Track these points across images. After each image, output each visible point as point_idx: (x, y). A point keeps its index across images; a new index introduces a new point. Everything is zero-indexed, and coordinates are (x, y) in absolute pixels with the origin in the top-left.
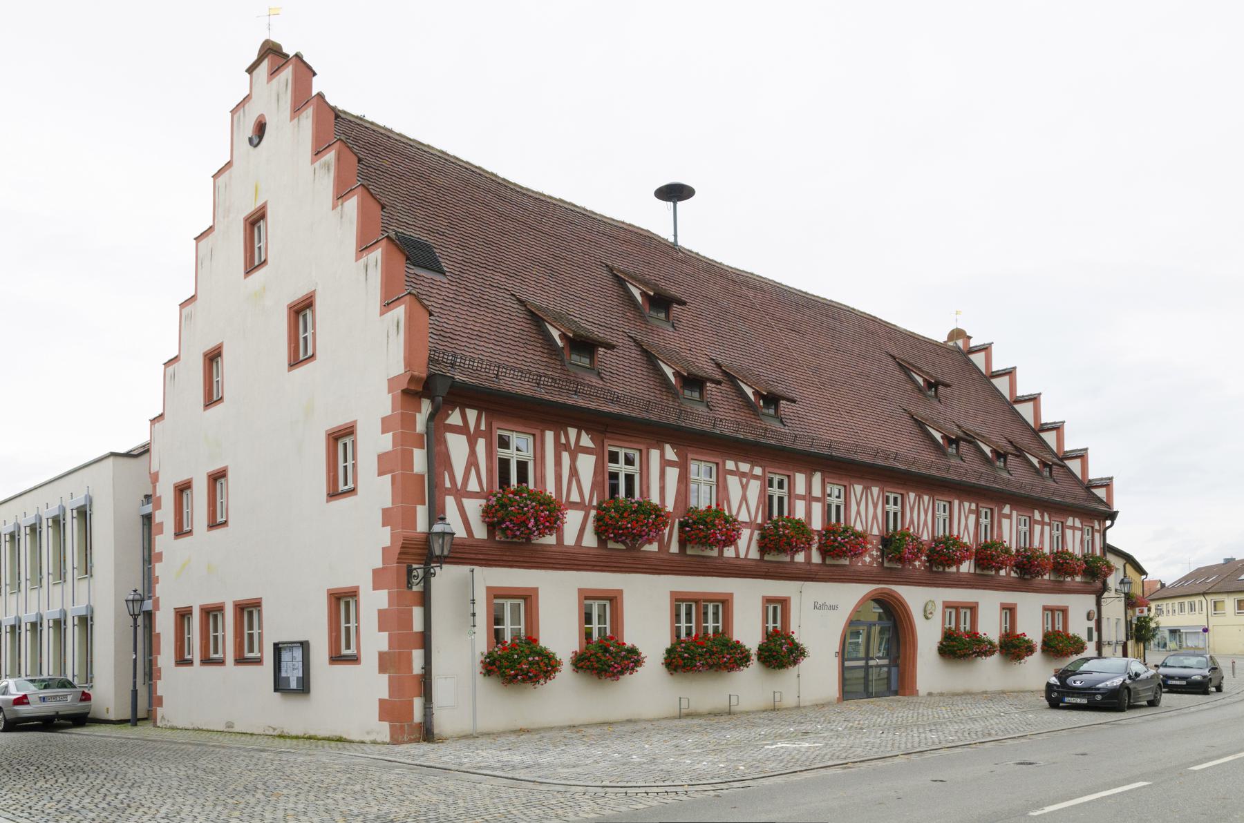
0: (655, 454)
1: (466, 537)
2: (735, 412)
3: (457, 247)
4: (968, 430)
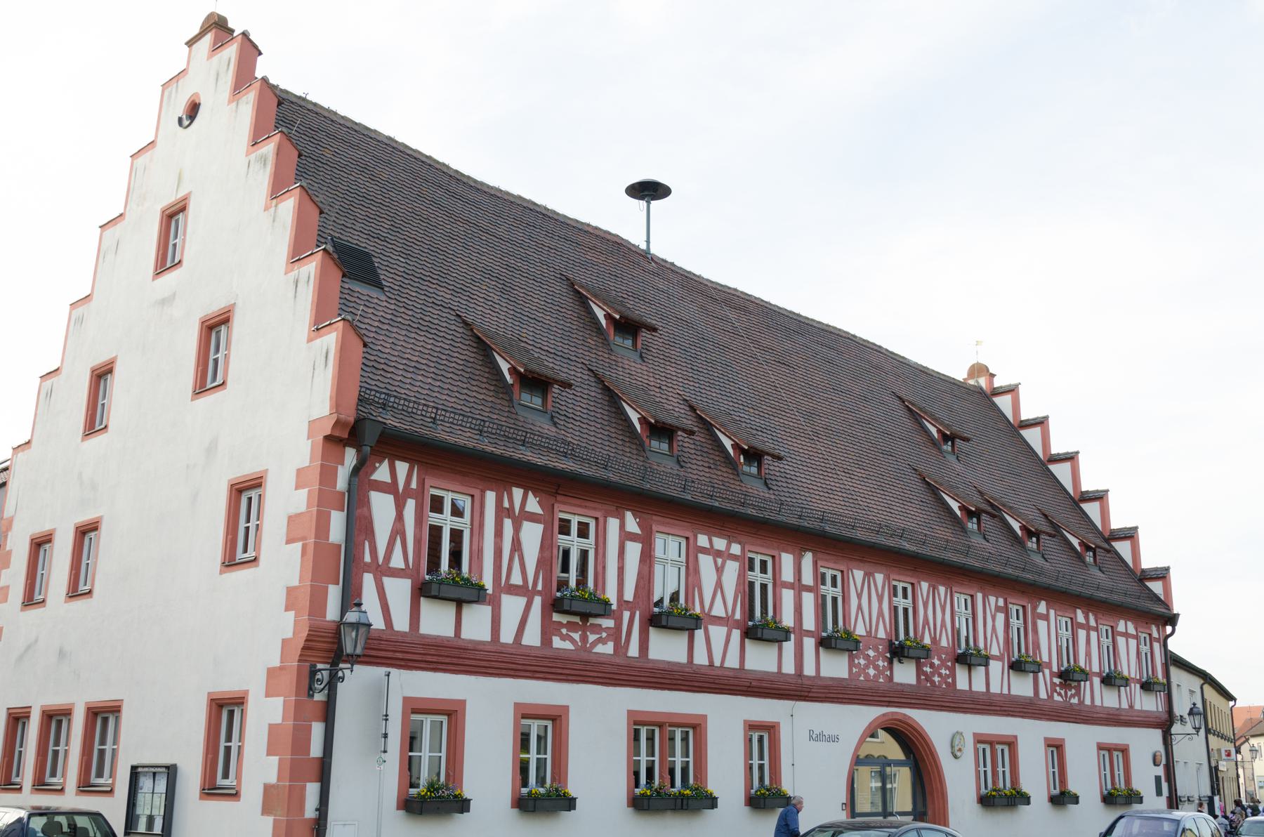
0: (613, 524)
1: (384, 628)
2: (710, 470)
3: (399, 255)
4: (992, 498)
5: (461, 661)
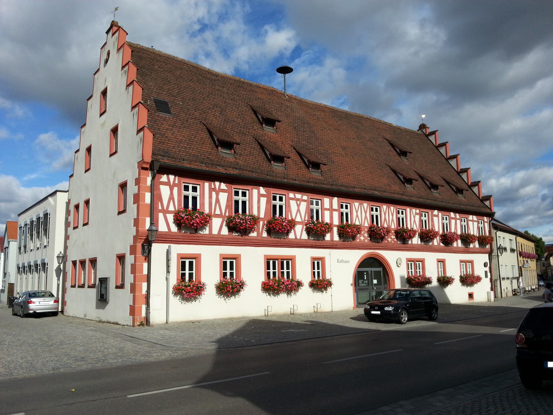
5: (200, 241)
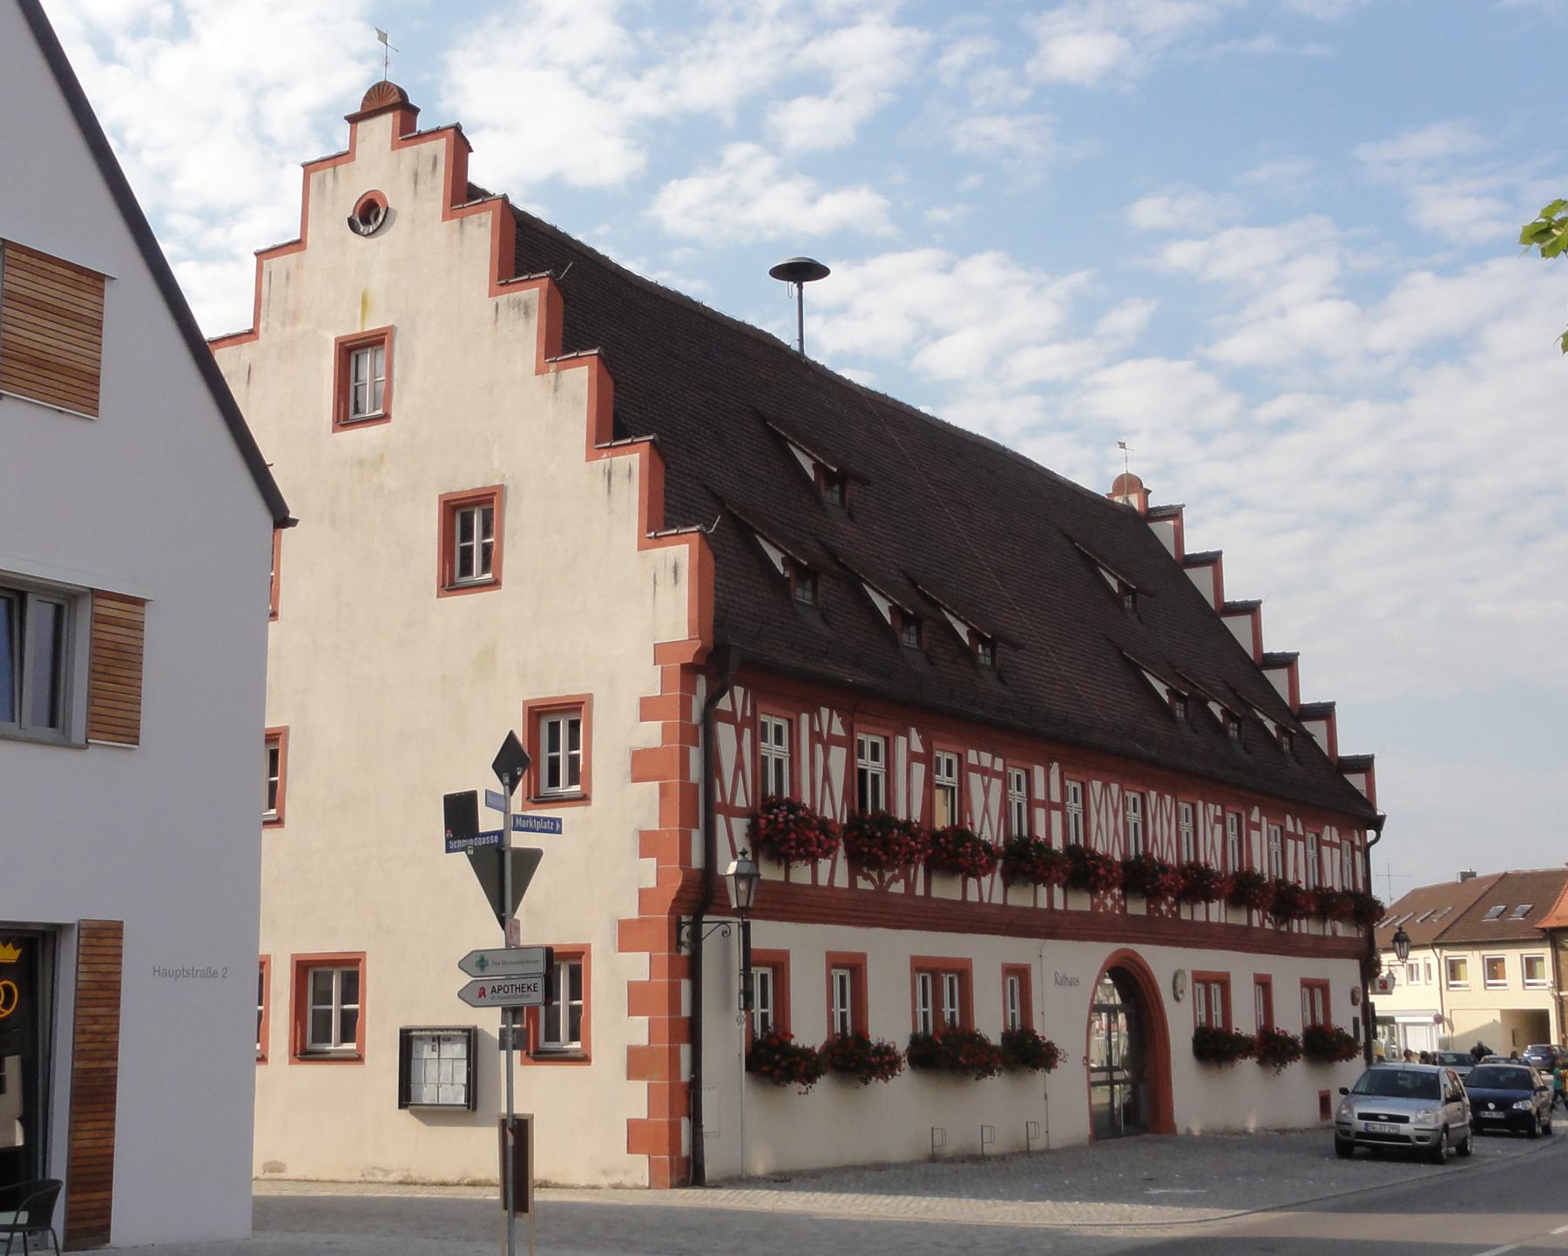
0: (901, 741)
